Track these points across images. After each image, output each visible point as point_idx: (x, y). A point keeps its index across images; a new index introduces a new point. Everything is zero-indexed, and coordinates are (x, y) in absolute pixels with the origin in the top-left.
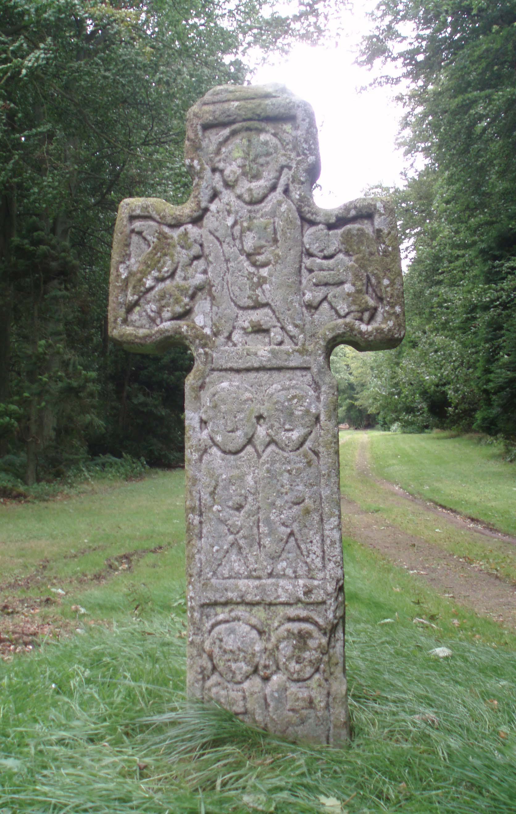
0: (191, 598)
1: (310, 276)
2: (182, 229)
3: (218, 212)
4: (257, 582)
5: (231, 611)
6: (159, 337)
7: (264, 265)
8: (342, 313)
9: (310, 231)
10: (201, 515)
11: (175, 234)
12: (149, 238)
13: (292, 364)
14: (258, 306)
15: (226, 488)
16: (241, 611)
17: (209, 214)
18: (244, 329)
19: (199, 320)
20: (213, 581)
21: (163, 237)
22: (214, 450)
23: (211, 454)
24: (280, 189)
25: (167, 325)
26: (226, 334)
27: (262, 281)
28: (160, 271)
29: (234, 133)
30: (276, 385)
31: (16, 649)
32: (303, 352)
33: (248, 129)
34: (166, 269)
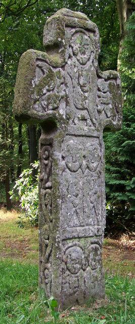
0: (58, 237)
1: (99, 99)
2: (58, 69)
3: (71, 65)
4: (83, 228)
5: (73, 242)
6: (47, 117)
7: (86, 92)
8: (109, 116)
9: (100, 80)
10: (62, 199)
11: (55, 71)
12: (45, 70)
13: (95, 135)
14: (84, 109)
15: (72, 187)
16: (76, 241)
17: (67, 65)
18: (79, 118)
19: (61, 112)
20: (68, 229)
21: (50, 71)
22: (67, 170)
23: (66, 172)
24: (91, 61)
25: (51, 112)
26: (72, 119)
27: (86, 98)
28: (49, 87)
29: (76, 32)
30: (89, 143)
31: (121, 105)
32: (98, 130)
33: (81, 32)
34: (51, 86)
